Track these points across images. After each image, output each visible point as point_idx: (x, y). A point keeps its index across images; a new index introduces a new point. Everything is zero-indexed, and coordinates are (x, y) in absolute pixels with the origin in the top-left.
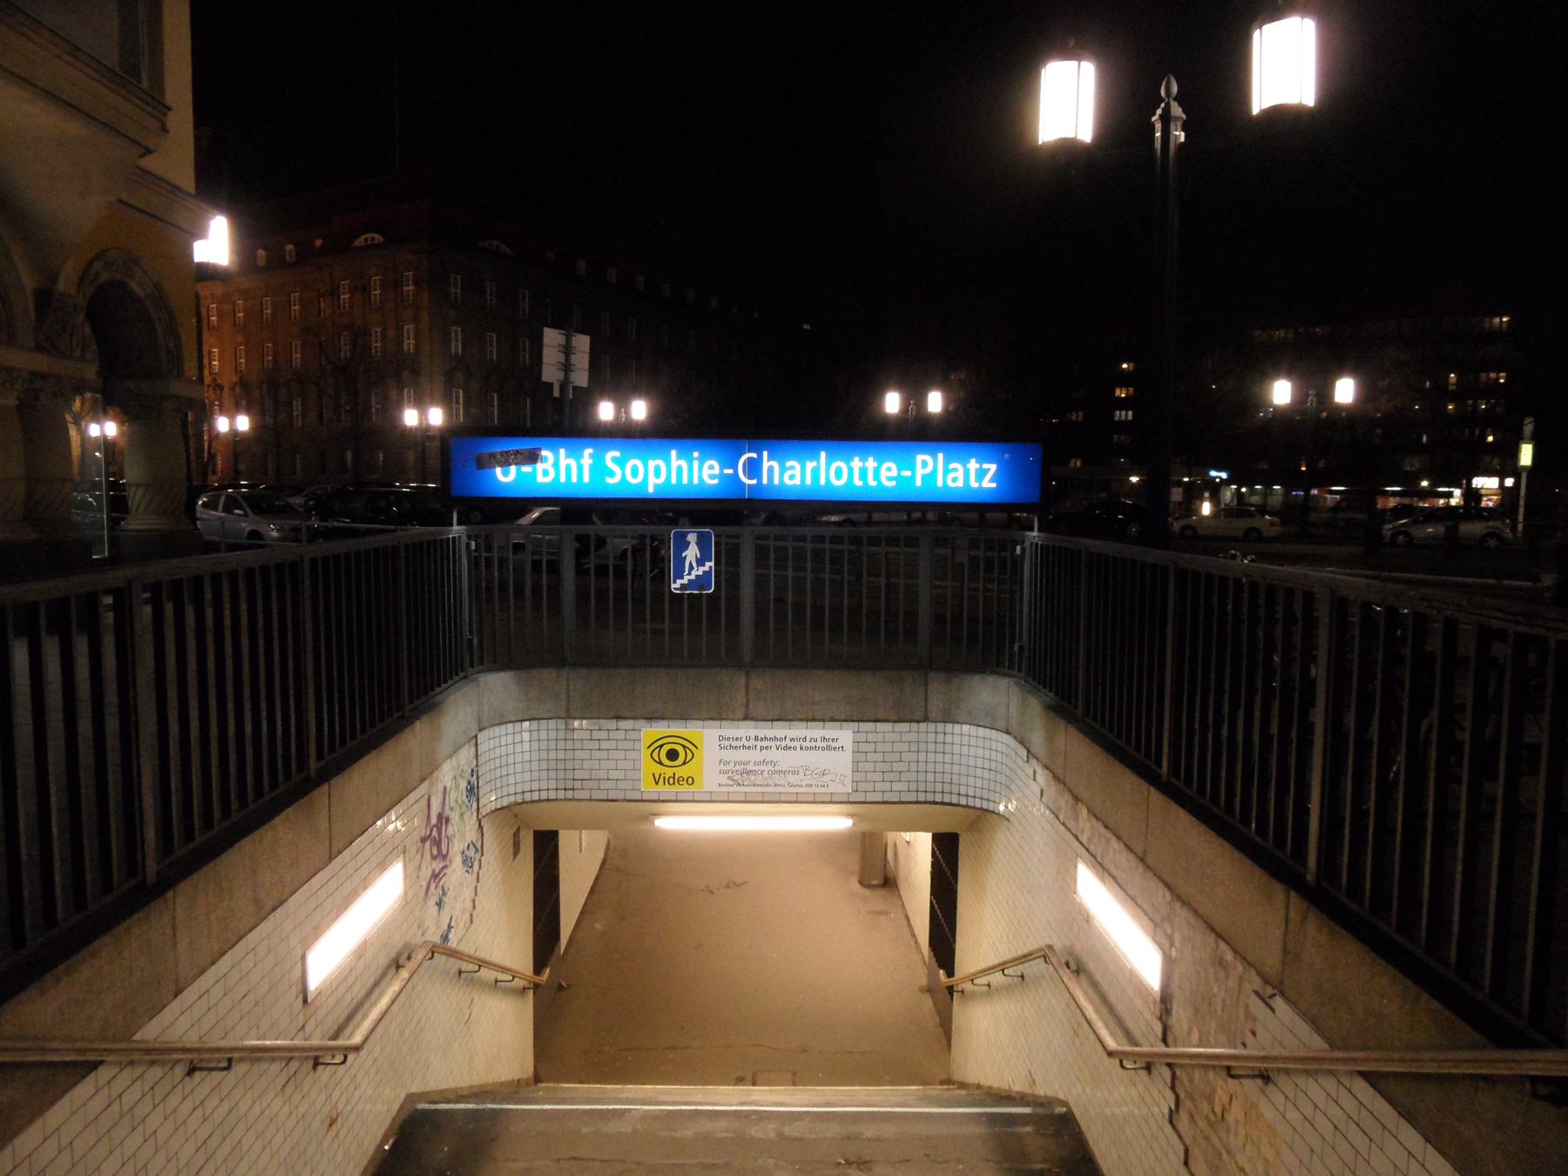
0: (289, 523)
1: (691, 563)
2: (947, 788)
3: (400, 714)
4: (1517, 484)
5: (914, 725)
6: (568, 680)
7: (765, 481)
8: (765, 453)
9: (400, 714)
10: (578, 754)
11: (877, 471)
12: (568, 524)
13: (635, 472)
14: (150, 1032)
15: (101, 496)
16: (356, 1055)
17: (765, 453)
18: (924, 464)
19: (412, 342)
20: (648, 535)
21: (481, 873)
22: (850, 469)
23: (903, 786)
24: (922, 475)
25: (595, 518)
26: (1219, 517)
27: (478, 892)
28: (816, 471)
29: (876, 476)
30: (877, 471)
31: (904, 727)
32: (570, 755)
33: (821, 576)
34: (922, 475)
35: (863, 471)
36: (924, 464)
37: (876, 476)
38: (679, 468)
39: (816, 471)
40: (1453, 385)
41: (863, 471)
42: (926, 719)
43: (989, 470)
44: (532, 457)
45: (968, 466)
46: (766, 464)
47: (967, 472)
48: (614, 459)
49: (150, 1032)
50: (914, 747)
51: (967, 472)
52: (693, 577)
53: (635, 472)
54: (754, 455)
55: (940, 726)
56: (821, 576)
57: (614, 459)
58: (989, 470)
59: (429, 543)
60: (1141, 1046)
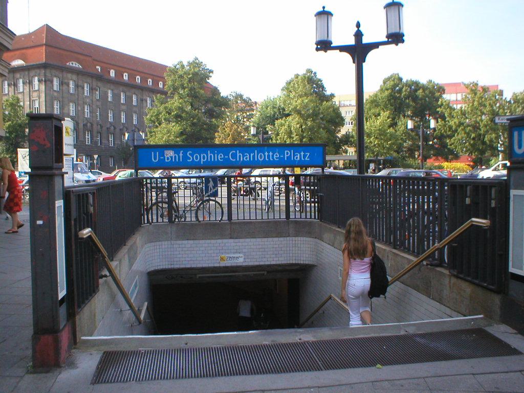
0: (267, 143)
2: (297, 258)
5: (285, 238)
6: (171, 227)
7: (238, 160)
10: (175, 253)
11: (273, 156)
14: (252, 174)
16: (389, 33)
18: (287, 154)
19: (86, 110)
22: (265, 156)
23: (283, 259)
28: (254, 157)
29: (273, 158)
30: (273, 156)
31: (282, 239)
32: (172, 253)
35: (269, 156)
36: (287, 154)
37: (273, 158)
38: (211, 156)
39: (254, 157)
41: (269, 156)
42: (289, 236)
44: (340, 131)
47: (300, 155)
49: (252, 174)
50: (285, 246)
51: (300, 155)
52: (211, 192)
55: (294, 238)
59: (83, 194)
60: (347, 305)
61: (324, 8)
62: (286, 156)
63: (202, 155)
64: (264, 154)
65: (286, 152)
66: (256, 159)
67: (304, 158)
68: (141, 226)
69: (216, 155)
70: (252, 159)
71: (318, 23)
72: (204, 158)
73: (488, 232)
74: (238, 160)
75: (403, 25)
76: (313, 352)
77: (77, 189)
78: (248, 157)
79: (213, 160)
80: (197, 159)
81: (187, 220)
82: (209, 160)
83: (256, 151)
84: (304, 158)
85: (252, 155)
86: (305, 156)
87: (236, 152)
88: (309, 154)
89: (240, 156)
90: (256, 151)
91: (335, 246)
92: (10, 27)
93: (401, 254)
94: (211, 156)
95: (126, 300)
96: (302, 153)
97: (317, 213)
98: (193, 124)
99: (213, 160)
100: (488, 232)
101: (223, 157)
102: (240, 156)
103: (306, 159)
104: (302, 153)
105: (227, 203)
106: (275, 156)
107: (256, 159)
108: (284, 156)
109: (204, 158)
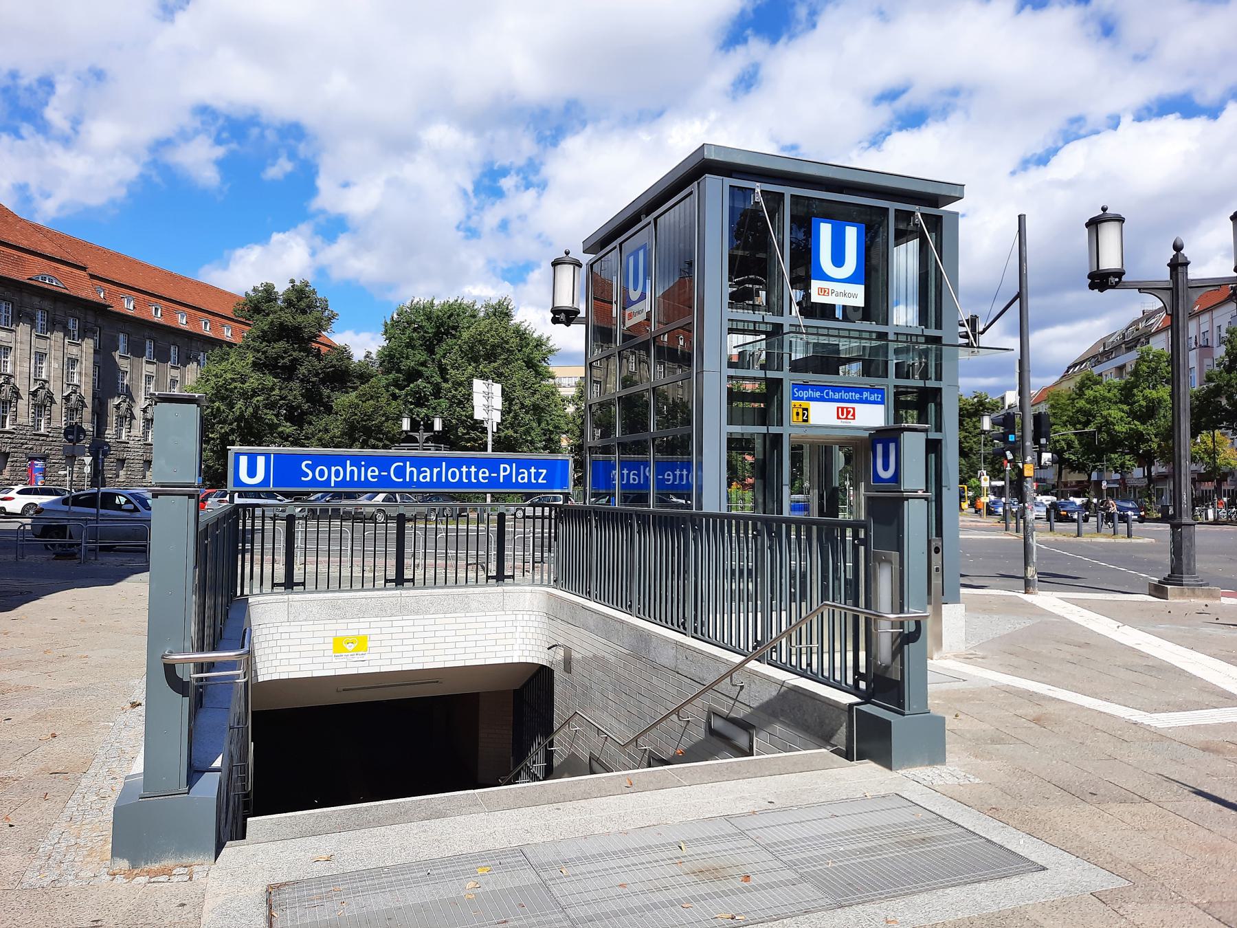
3: (425, 335)
4: (119, 507)
7: (408, 480)
8: (408, 463)
9: (425, 335)
13: (322, 473)
15: (493, 495)
17: (408, 463)
18: (505, 469)
21: (83, 273)
22: (461, 473)
24: (504, 476)
27: (95, 281)
34: (504, 476)
35: (469, 474)
36: (505, 469)
38: (352, 472)
39: (439, 474)
40: (572, 400)
41: (469, 474)
43: (542, 473)
45: (531, 470)
47: (530, 474)
51: (530, 474)
53: (322, 473)
54: (402, 464)
57: (307, 466)
58: (542, 473)
61: (1104, 209)
62: (502, 474)
63: (333, 469)
64: (673, 473)
65: (502, 466)
66: (444, 480)
67: (537, 478)
69: (363, 469)
70: (435, 480)
71: (794, 226)
72: (337, 475)
74: (408, 480)
75: (132, 263)
77: (240, 563)
78: (428, 474)
80: (453, 473)
81: (264, 592)
82: (348, 479)
83: (444, 463)
84: (537, 478)
85: (435, 470)
87: (405, 465)
88: (545, 471)
89: (412, 472)
91: (387, 584)
94: (352, 472)
95: (896, 713)
98: (1052, 406)
101: (487, 475)
102: (412, 472)
103: (540, 481)
104: (533, 470)
106: (481, 475)
107: (444, 480)
109: (337, 475)
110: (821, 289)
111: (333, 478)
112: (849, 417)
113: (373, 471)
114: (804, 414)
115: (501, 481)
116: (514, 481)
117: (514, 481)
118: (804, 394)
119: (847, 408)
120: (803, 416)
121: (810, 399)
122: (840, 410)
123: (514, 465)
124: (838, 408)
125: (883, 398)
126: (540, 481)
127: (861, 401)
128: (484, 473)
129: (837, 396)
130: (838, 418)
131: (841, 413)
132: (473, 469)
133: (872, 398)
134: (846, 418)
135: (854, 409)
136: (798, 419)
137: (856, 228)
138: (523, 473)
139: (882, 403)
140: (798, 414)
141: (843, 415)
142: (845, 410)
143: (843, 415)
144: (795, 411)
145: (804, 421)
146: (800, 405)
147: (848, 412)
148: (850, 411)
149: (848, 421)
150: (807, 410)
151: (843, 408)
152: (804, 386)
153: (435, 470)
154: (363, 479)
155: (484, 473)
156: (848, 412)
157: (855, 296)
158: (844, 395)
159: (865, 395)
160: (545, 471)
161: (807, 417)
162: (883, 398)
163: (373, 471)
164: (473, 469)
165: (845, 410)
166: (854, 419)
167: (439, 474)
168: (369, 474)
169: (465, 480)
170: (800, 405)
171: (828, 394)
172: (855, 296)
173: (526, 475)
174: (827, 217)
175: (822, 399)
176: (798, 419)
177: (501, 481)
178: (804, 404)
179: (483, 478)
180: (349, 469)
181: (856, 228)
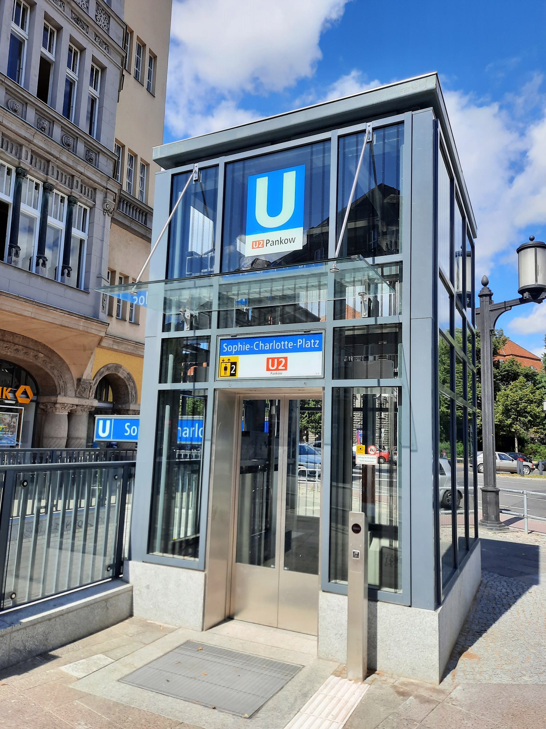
1: (369, 131)
7: (260, 349)
8: (261, 342)
11: (288, 344)
12: (125, 509)
17: (261, 342)
18: (300, 342)
20: (127, 323)
25: (361, 224)
26: (539, 382)
30: (288, 344)
33: (186, 327)
35: (284, 344)
36: (300, 342)
39: (273, 345)
41: (284, 344)
46: (261, 344)
47: (311, 343)
48: (128, 426)
51: (311, 343)
56: (186, 327)
57: (128, 426)
62: (299, 344)
67: (314, 345)
68: (332, 24)
73: (177, 457)
76: (15, 90)
78: (268, 346)
79: (242, 350)
83: (274, 341)
84: (314, 345)
85: (271, 344)
86: (315, 343)
88: (318, 341)
89: (262, 346)
90: (274, 341)
92: (18, 245)
93: (180, 705)
96: (313, 341)
97: (128, 489)
99: (242, 350)
100: (177, 457)
101: (292, 345)
102: (262, 346)
103: (316, 346)
105: (51, 539)
106: (289, 345)
108: (297, 345)
110: (256, 242)
111: (234, 350)
112: (280, 368)
113: (248, 346)
114: (232, 368)
115: (298, 347)
116: (304, 347)
117: (304, 347)
118: (234, 348)
119: (278, 358)
120: (231, 371)
121: (238, 353)
122: (270, 360)
123: (304, 339)
124: (268, 359)
125: (320, 344)
126: (316, 346)
127: (295, 350)
128: (291, 344)
129: (268, 347)
130: (268, 369)
131: (271, 365)
132: (286, 343)
133: (308, 345)
134: (277, 369)
135: (286, 359)
136: (225, 373)
137: (285, 174)
138: (308, 343)
139: (319, 349)
140: (226, 369)
141: (273, 366)
142: (276, 360)
143: (273, 366)
144: (223, 365)
145: (232, 375)
146: (229, 360)
147: (279, 363)
148: (282, 361)
149: (278, 372)
150: (235, 363)
151: (273, 359)
152: (234, 339)
153: (271, 344)
154: (244, 350)
155: (291, 344)
156: (279, 363)
157: (293, 240)
158: (276, 345)
159: (300, 342)
160: (318, 341)
161: (235, 371)
162: (320, 344)
163: (248, 346)
164: (286, 343)
165: (276, 360)
166: (286, 369)
167: (273, 345)
168: (246, 347)
169: (283, 348)
170: (229, 360)
171: (257, 346)
172: (293, 240)
173: (309, 344)
174: (261, 172)
175: (251, 352)
176: (225, 373)
177: (298, 347)
178: (233, 358)
179: (291, 346)
180: (239, 346)
181: (285, 174)
